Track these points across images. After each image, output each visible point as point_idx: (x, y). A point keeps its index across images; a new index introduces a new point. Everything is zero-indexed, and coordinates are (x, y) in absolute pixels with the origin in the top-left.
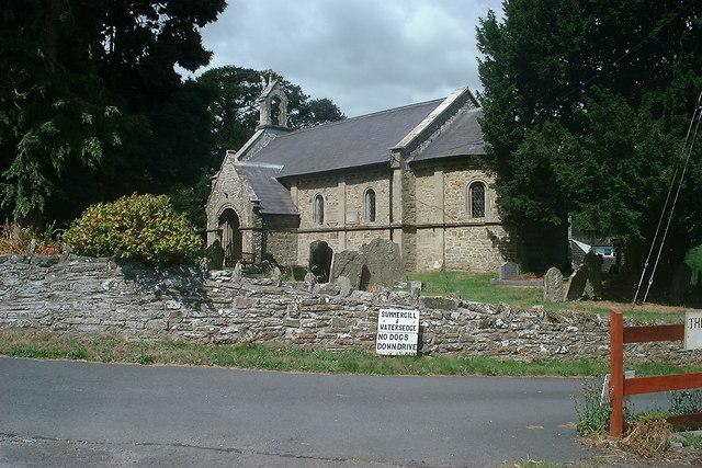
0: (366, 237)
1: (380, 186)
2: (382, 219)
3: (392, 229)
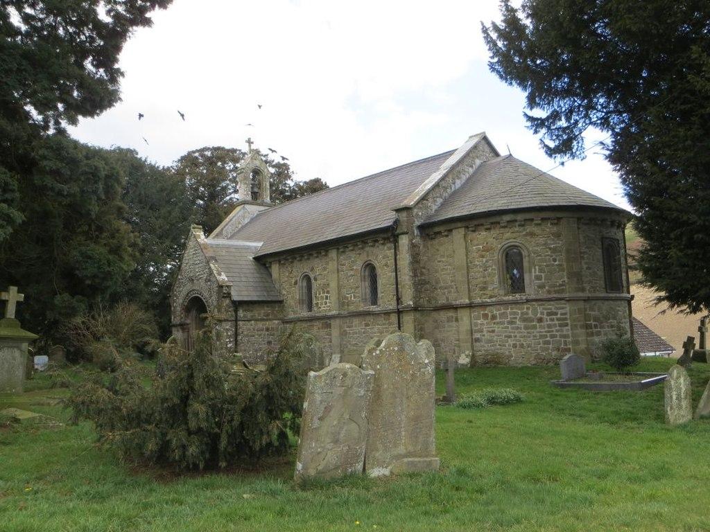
0: (367, 325)
1: (381, 256)
2: (387, 301)
3: (399, 312)
